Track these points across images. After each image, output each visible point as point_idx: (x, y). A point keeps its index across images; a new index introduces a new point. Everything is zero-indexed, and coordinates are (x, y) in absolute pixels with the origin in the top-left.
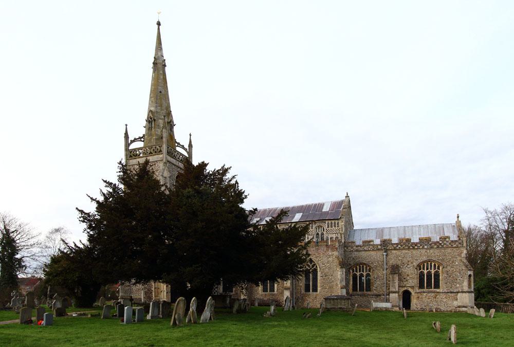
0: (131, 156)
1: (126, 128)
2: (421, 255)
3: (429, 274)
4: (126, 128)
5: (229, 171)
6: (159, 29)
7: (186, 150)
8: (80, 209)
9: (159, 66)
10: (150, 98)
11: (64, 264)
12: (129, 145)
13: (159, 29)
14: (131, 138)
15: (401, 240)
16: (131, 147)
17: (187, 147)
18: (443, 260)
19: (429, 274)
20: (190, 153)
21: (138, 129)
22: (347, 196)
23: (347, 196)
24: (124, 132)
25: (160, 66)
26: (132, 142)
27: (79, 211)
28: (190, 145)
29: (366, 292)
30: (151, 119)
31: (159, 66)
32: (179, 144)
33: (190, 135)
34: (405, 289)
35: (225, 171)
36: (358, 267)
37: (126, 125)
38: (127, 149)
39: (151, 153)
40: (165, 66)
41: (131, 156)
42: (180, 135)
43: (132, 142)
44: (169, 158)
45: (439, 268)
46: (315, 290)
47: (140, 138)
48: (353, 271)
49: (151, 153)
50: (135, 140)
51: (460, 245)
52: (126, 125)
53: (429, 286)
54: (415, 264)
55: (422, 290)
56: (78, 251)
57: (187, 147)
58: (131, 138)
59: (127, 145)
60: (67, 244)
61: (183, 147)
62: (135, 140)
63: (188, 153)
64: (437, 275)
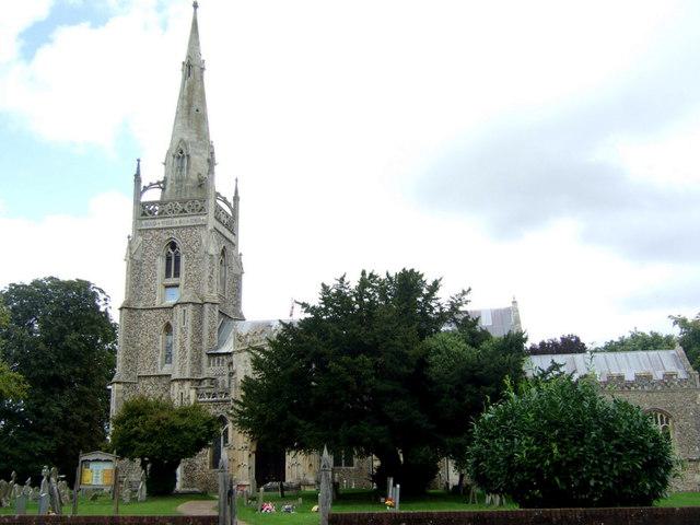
0: (144, 214)
1: (138, 168)
4: (138, 168)
5: (440, 283)
6: (195, 13)
8: (207, 52)
9: (193, 70)
10: (177, 113)
12: (142, 193)
13: (195, 13)
14: (145, 183)
17: (230, 200)
18: (672, 409)
20: (235, 210)
21: (155, 171)
22: (514, 302)
23: (514, 302)
25: (196, 69)
26: (146, 188)
27: (236, 192)
28: (236, 198)
30: (181, 153)
31: (193, 70)
37: (139, 160)
38: (137, 201)
39: (184, 211)
40: (203, 69)
41: (144, 214)
42: (222, 184)
43: (146, 188)
45: (667, 423)
47: (158, 183)
49: (184, 211)
51: (692, 386)
52: (139, 160)
57: (230, 200)
59: (139, 192)
61: (225, 201)
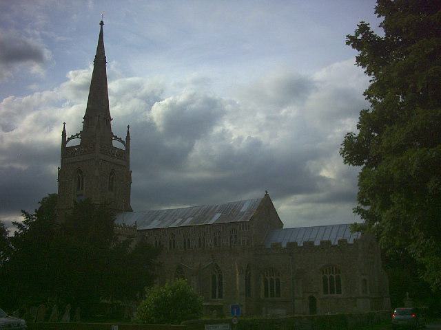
3: (272, 281)
7: (123, 142)
15: (305, 243)
16: (68, 146)
17: (124, 139)
19: (272, 281)
22: (266, 195)
26: (69, 139)
28: (128, 138)
34: (311, 294)
35: (378, 17)
37: (64, 123)
43: (69, 139)
47: (77, 135)
53: (332, 292)
55: (326, 295)
57: (124, 139)
60: (72, 136)
61: (120, 140)
64: (338, 280)
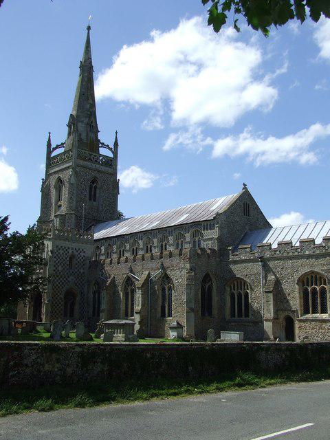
2: (304, 268)
6: (89, 33)
7: (111, 149)
11: (255, 21)
13: (89, 33)
14: (53, 146)
16: (53, 154)
17: (112, 146)
20: (115, 153)
21: (61, 135)
24: (80, 57)
26: (54, 149)
28: (116, 144)
29: (245, 319)
32: (103, 144)
33: (116, 133)
34: (286, 313)
36: (236, 283)
37: (50, 133)
42: (105, 136)
44: (81, 162)
46: (170, 315)
47: (62, 144)
48: (231, 289)
50: (58, 147)
54: (296, 278)
56: (141, 167)
57: (112, 146)
58: (53, 146)
59: (49, 153)
62: (58, 147)
63: (113, 153)
